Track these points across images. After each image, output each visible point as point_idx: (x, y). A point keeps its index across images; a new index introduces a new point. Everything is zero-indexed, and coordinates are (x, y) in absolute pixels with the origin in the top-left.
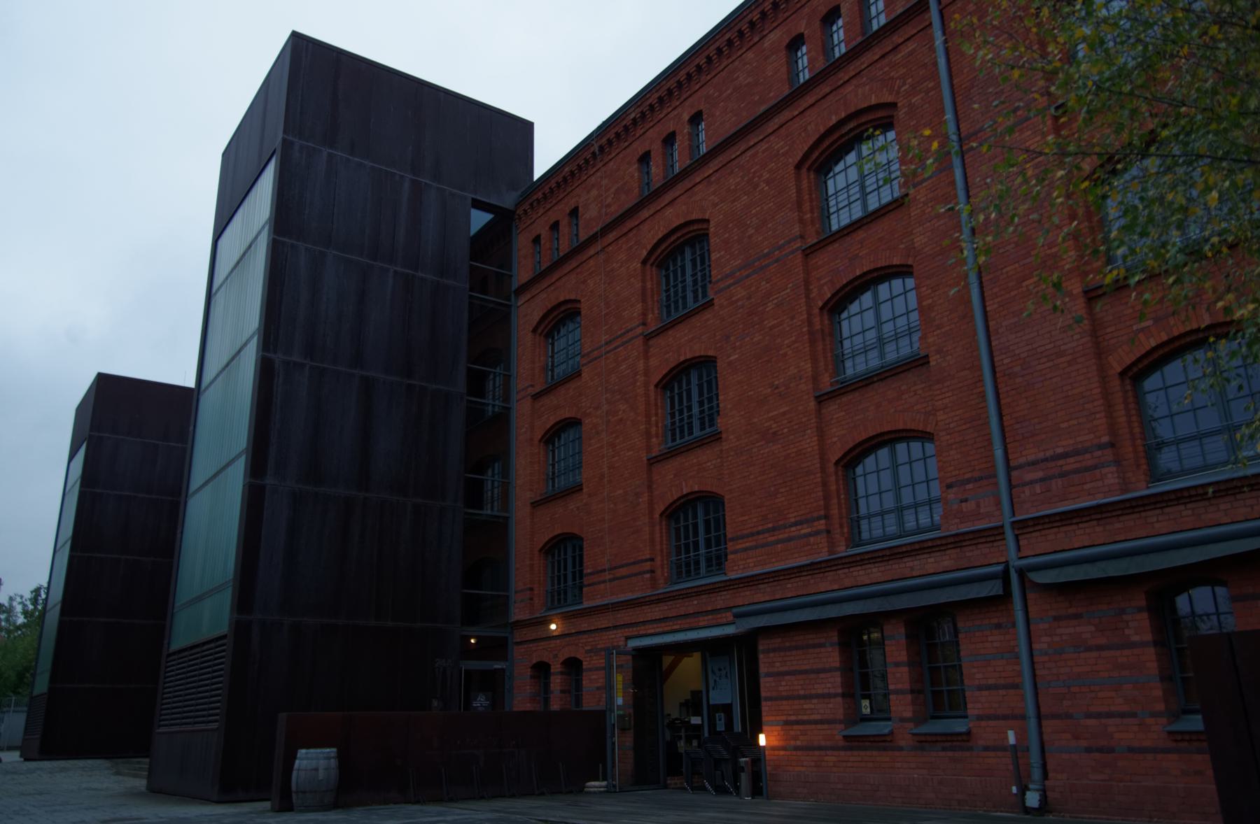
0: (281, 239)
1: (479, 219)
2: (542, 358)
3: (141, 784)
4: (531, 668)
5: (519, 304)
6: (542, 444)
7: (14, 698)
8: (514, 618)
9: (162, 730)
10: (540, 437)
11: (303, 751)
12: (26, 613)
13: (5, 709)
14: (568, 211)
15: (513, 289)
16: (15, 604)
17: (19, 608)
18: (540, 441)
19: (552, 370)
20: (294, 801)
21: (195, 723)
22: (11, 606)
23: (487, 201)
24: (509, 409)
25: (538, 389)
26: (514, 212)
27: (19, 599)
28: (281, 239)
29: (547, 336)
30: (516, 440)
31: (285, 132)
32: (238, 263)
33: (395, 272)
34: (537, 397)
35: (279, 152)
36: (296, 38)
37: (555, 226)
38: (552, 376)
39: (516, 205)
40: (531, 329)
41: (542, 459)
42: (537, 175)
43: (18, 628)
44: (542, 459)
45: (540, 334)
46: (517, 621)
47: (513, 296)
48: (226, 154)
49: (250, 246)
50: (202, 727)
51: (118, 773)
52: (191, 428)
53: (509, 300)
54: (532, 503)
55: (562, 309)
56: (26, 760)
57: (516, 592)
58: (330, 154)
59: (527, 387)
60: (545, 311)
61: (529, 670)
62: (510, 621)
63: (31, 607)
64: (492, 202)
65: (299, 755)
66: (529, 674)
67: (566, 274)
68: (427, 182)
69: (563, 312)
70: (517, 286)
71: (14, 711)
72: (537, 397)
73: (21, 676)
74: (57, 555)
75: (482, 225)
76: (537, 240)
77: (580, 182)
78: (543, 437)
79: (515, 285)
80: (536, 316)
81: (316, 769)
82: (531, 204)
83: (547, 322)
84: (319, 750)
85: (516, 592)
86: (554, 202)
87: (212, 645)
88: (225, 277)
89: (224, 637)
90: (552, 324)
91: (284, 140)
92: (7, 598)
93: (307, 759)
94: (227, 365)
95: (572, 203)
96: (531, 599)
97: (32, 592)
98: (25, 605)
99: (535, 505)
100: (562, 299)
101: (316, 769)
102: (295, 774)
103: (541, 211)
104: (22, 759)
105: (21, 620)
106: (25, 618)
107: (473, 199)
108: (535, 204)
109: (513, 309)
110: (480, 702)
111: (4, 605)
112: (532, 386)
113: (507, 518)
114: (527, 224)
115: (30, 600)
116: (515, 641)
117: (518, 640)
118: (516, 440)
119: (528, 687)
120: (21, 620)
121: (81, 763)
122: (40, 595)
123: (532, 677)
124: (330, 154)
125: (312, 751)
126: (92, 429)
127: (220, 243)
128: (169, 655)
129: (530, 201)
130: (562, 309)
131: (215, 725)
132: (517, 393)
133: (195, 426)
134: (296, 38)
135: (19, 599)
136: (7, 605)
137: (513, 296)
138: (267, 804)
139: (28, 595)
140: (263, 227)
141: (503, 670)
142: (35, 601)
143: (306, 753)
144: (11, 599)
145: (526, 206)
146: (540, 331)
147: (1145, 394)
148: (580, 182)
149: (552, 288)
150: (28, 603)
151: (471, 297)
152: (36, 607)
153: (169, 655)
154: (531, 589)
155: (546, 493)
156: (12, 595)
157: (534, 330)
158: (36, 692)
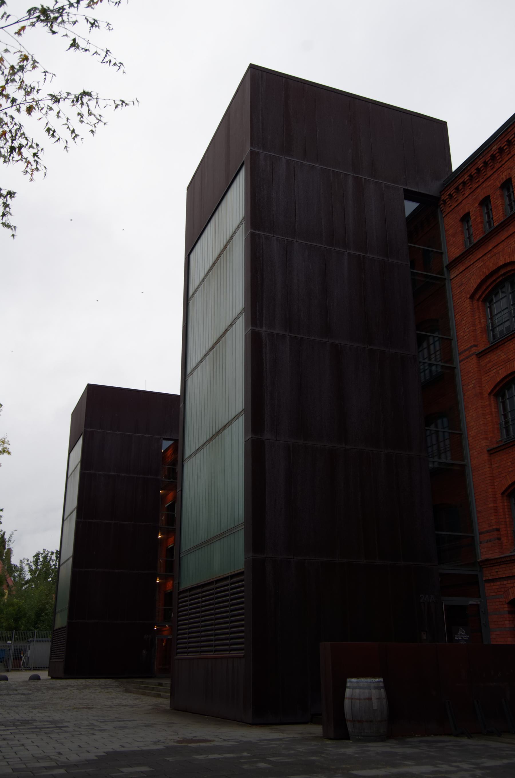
0: (257, 232)
1: (410, 207)
2: (482, 321)
3: (165, 702)
4: (508, 603)
5: (452, 277)
6: (492, 397)
7: (36, 631)
8: (481, 558)
9: (179, 656)
10: (489, 390)
11: (354, 680)
12: (31, 571)
13: (30, 639)
14: (499, 185)
15: (445, 264)
16: (24, 565)
17: (27, 568)
18: (490, 394)
19: (493, 330)
20: (350, 729)
21: (216, 651)
22: (21, 566)
23: (417, 190)
24: (453, 369)
25: (482, 348)
26: (438, 199)
27: (26, 562)
28: (257, 232)
29: (484, 301)
30: (464, 395)
31: (252, 145)
32: (214, 264)
33: (349, 254)
34: (480, 355)
35: (248, 163)
36: (252, 67)
37: (486, 202)
38: (494, 336)
39: (441, 192)
40: (468, 296)
41: (493, 410)
42: (455, 166)
43: (27, 582)
44: (493, 410)
45: (478, 300)
46: (488, 560)
47: (445, 270)
48: (191, 189)
49: (225, 247)
50: (226, 654)
51: (127, 691)
52: (181, 405)
53: (443, 274)
54: (488, 451)
55: (502, 272)
56: (52, 678)
57: (480, 534)
58: (287, 160)
59: (471, 347)
60: (483, 278)
61: (506, 606)
62: (478, 560)
63: (34, 567)
64: (420, 191)
65: (348, 684)
66: (507, 609)
67: (503, 241)
68: (366, 178)
69: (502, 275)
70: (448, 263)
71: (37, 641)
72: (480, 355)
73: (38, 615)
74: (65, 522)
75: (146, 390)
76: (466, 218)
77: (510, 156)
78: (492, 391)
79: (446, 261)
80: (473, 284)
81: (370, 699)
82: (457, 189)
83: (485, 287)
84: (369, 680)
85: (480, 534)
86: (482, 181)
87: (228, 582)
88: (201, 279)
89: (242, 573)
90: (491, 288)
91: (252, 152)
92: (19, 561)
93: (360, 688)
94: (213, 347)
95: (504, 177)
96: (499, 539)
97: (34, 557)
98: (30, 566)
99: (492, 452)
100: (501, 263)
101: (370, 699)
102: (347, 703)
103: (467, 192)
104: (50, 677)
105: (28, 576)
106: (31, 575)
107: (404, 189)
108: (460, 187)
109: (447, 282)
110: (461, 635)
111: (16, 566)
112: (476, 346)
113: (463, 466)
114: (452, 207)
115: (33, 562)
116: (484, 578)
117: (490, 578)
118: (464, 395)
119: (507, 622)
120: (28, 576)
121: (96, 682)
122: (39, 559)
123: (510, 612)
124: (287, 160)
125: (363, 680)
126: (86, 426)
127: (192, 256)
128: (180, 593)
129: (456, 185)
130: (502, 272)
131: (241, 653)
132: (459, 354)
133: (184, 404)
134: (252, 67)
135: (26, 562)
136: (18, 566)
137: (445, 270)
138: (317, 730)
139: (32, 559)
140: (241, 223)
141: (477, 606)
142: (36, 562)
143: (357, 683)
144: (21, 562)
145: (452, 190)
146: (477, 296)
147: (244, 528)
148: (510, 156)
149: (489, 256)
150: (32, 564)
151: (413, 274)
152: (37, 567)
153: (180, 593)
154: (498, 530)
155: (501, 441)
156: (22, 559)
157: (472, 297)
158: (58, 625)
